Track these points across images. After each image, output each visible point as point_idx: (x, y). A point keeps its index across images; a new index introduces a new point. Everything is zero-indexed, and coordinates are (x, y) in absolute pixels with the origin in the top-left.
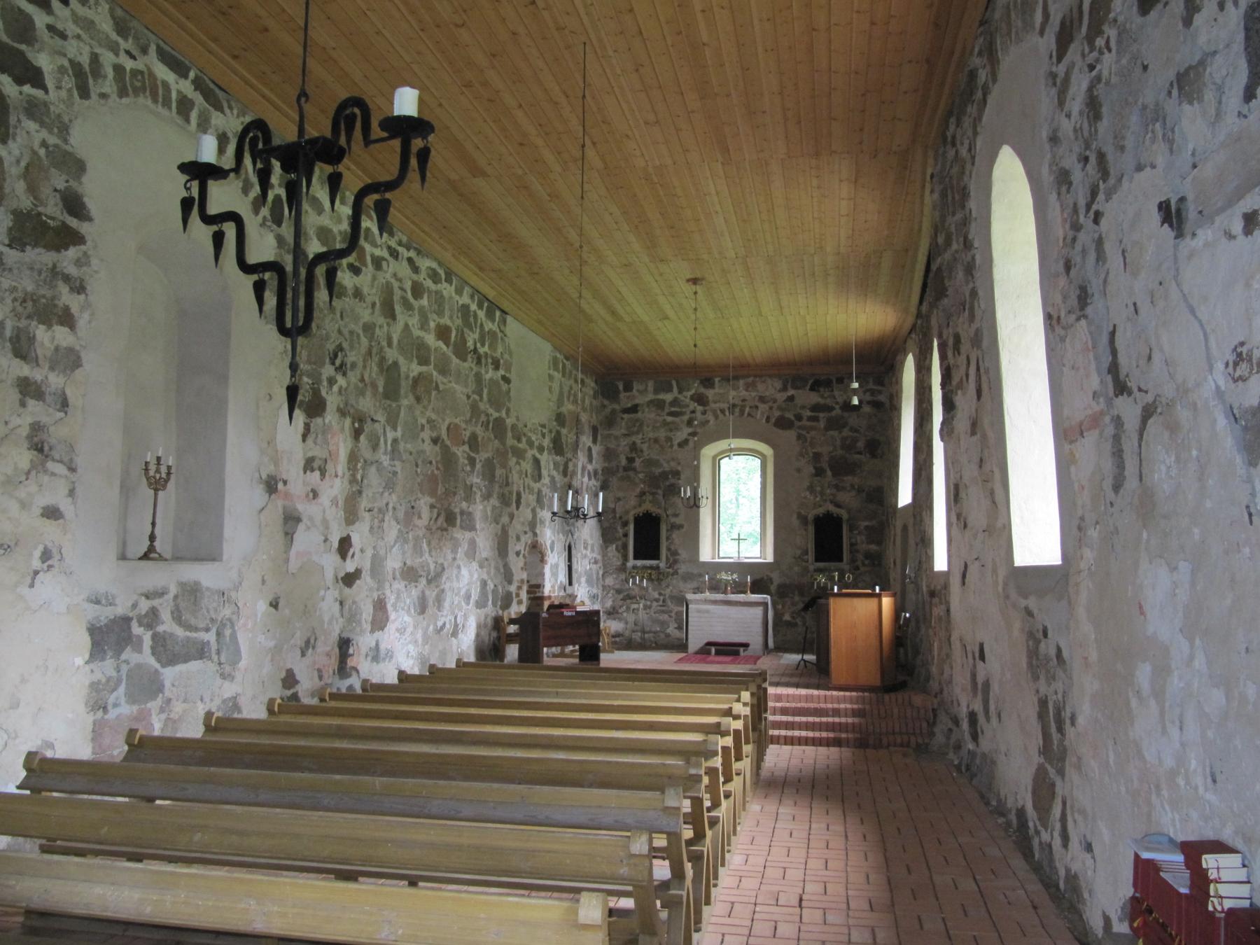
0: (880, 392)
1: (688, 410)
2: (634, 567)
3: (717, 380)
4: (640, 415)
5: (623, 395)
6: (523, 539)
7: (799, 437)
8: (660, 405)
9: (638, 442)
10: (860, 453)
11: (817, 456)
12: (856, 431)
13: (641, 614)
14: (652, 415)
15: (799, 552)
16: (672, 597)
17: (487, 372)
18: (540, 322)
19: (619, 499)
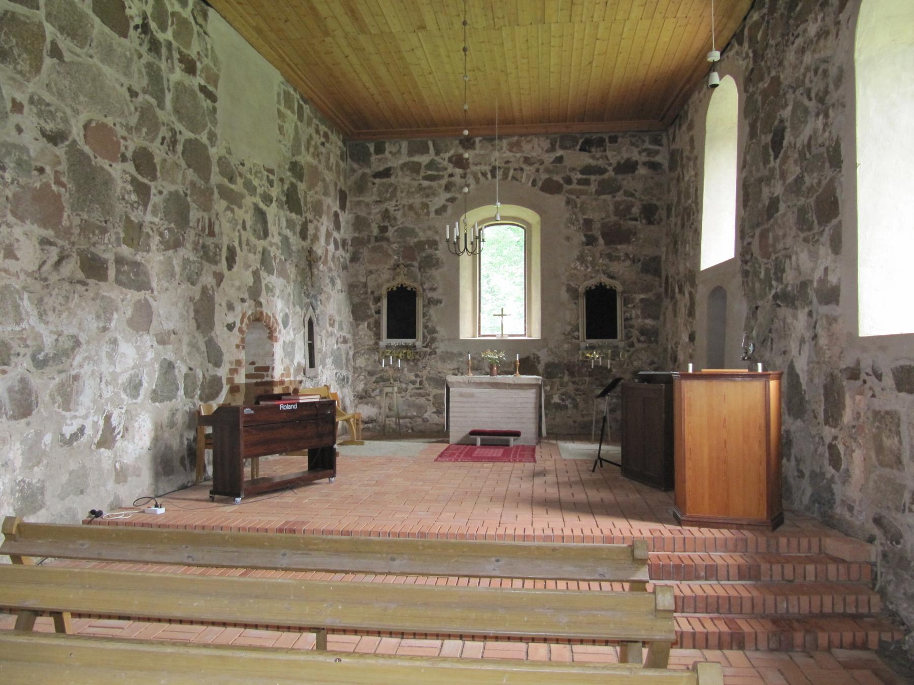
0: (657, 152)
1: (446, 174)
2: (388, 347)
3: (477, 140)
4: (387, 154)
5: (373, 158)
6: (239, 307)
7: (568, 202)
8: (415, 168)
9: (391, 209)
10: (635, 219)
11: (588, 223)
12: (632, 195)
13: (397, 398)
14: (407, 180)
15: (568, 328)
16: (429, 379)
17: (172, 70)
18: (259, 31)
19: (371, 272)
